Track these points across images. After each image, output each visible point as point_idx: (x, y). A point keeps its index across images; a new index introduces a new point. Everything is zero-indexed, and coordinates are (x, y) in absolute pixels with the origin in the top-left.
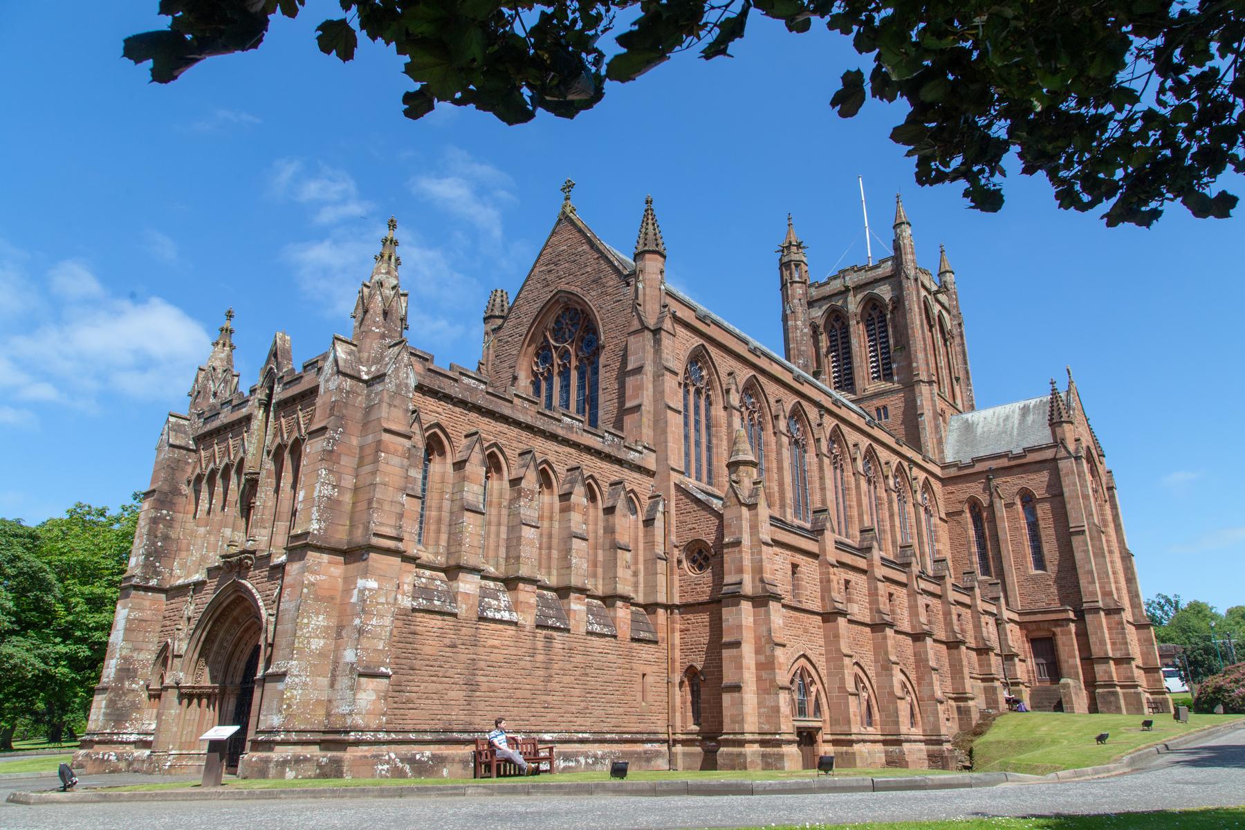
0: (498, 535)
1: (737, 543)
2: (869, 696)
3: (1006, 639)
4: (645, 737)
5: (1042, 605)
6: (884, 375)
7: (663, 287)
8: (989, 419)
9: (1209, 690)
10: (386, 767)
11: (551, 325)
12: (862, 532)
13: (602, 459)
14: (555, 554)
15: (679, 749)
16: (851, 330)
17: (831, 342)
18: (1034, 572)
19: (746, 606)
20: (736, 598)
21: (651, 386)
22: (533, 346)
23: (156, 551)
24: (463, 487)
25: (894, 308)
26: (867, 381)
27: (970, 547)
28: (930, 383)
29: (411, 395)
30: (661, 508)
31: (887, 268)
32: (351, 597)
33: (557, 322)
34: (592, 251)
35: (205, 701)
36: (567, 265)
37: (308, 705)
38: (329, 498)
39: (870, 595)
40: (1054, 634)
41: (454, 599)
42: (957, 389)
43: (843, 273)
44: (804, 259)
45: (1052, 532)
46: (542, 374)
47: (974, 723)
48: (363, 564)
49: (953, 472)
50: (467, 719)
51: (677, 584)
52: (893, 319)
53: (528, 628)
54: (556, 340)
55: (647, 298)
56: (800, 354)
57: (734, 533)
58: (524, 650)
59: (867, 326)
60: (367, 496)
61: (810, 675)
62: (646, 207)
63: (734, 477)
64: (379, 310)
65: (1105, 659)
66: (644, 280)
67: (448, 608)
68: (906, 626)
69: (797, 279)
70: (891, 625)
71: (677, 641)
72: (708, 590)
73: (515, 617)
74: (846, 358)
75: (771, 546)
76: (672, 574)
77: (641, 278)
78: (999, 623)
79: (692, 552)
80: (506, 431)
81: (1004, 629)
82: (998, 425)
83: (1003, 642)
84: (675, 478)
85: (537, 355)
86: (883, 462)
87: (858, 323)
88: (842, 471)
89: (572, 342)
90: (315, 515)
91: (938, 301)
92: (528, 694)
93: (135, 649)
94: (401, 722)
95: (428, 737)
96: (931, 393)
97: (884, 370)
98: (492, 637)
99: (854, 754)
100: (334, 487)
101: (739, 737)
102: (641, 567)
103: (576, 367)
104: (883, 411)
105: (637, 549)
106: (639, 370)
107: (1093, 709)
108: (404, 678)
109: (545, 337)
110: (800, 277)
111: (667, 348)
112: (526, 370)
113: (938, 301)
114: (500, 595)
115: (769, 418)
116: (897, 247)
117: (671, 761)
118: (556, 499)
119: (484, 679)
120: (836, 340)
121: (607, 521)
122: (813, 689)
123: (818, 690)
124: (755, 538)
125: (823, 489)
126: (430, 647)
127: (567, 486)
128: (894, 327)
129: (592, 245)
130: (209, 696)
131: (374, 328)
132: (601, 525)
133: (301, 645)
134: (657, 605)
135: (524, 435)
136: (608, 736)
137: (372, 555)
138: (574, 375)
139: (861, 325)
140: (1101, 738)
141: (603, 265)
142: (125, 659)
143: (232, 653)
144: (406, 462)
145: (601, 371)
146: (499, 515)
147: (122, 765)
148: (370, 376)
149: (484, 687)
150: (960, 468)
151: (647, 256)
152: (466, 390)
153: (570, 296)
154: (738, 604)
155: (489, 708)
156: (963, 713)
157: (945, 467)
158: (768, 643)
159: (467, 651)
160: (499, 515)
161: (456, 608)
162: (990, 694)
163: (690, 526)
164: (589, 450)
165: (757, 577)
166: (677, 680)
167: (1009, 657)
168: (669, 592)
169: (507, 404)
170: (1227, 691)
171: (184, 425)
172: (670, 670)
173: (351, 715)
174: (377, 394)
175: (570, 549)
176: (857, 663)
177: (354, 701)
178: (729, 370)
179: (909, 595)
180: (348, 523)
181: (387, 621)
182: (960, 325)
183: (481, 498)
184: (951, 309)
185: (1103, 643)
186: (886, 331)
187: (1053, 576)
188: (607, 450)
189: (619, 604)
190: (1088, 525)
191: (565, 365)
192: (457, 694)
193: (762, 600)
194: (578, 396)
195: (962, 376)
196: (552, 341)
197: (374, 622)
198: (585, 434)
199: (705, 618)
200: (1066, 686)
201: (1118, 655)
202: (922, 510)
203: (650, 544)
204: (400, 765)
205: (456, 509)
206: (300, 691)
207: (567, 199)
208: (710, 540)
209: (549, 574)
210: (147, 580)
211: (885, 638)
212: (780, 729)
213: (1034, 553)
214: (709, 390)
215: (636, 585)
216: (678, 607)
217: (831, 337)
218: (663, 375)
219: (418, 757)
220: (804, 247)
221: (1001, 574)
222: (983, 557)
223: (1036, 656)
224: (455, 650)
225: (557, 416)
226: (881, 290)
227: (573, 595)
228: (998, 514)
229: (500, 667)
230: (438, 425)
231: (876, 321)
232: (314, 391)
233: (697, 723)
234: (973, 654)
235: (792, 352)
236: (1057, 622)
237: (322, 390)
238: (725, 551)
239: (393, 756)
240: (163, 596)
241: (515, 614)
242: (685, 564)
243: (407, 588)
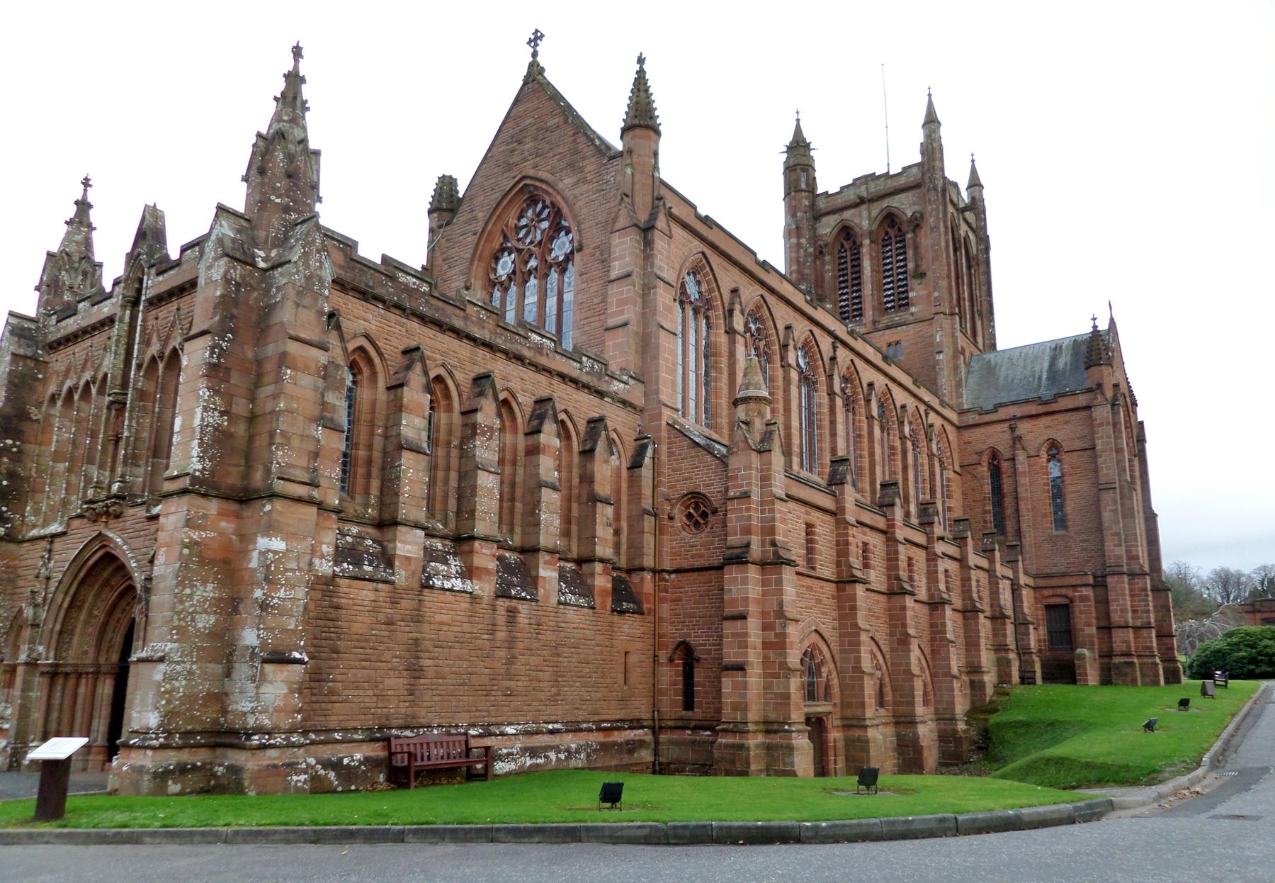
0: (446, 481)
1: (746, 496)
2: (882, 674)
3: (1022, 607)
10: (303, 777)
14: (519, 506)
19: (753, 573)
24: (400, 419)
29: (327, 293)
30: (649, 453)
32: (250, 561)
37: (196, 699)
38: (216, 429)
41: (390, 563)
42: (979, 323)
47: (988, 698)
50: (409, 711)
53: (486, 600)
55: (636, 187)
58: (481, 626)
60: (267, 428)
61: (821, 652)
67: (382, 574)
70: (912, 594)
73: (468, 586)
75: (786, 501)
81: (1020, 596)
83: (1018, 609)
88: (854, 414)
90: (195, 451)
92: (485, 679)
94: (323, 718)
100: (222, 414)
102: (624, 524)
105: (619, 500)
107: (1106, 680)
108: (323, 664)
111: (661, 253)
114: (450, 558)
115: (776, 347)
118: (521, 436)
119: (429, 662)
120: (846, 262)
122: (824, 670)
123: (829, 671)
125: (833, 435)
126: (359, 624)
131: (273, 197)
132: (576, 472)
133: (182, 623)
135: (481, 353)
144: (320, 383)
146: (448, 457)
148: (269, 264)
149: (430, 672)
152: (404, 291)
155: (437, 698)
157: (962, 412)
158: (776, 618)
159: (407, 629)
160: (448, 457)
161: (393, 574)
164: (563, 377)
168: (657, 554)
169: (458, 312)
171: (30, 329)
173: (253, 713)
174: (279, 289)
175: (539, 502)
177: (257, 697)
178: (733, 286)
180: (243, 462)
181: (300, 592)
183: (424, 435)
188: (585, 378)
190: (1120, 481)
192: (395, 683)
197: (282, 594)
198: (558, 357)
200: (1082, 657)
201: (1138, 623)
203: (635, 494)
204: (322, 772)
205: (390, 448)
206: (184, 683)
209: (512, 531)
212: (790, 719)
214: (708, 309)
215: (617, 546)
218: (655, 287)
219: (346, 761)
224: (392, 628)
229: (450, 647)
230: (367, 337)
231: (893, 240)
232: (193, 284)
237: (201, 282)
239: (312, 761)
241: (468, 582)
243: (327, 549)
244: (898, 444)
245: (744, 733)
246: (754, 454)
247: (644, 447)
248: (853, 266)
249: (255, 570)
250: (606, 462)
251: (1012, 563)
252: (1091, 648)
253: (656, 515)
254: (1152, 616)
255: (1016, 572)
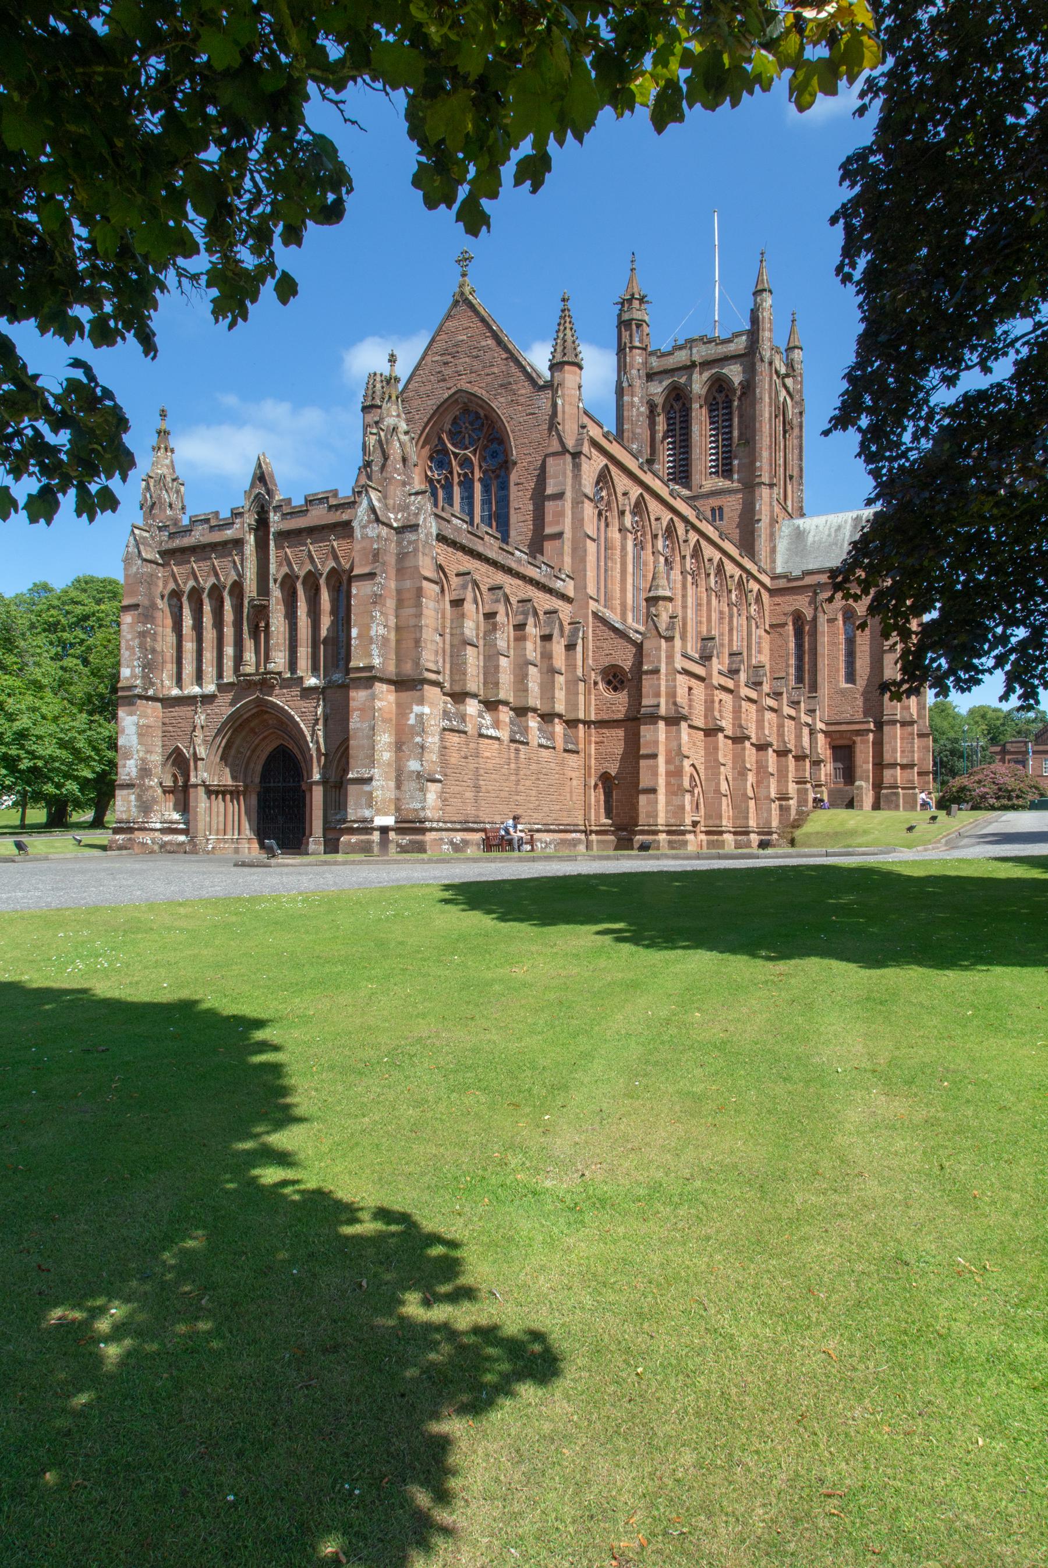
1: (656, 671)
3: (816, 747)
4: (572, 828)
5: (846, 716)
6: (723, 471)
7: (581, 405)
8: (821, 528)
9: (954, 789)
11: (447, 427)
12: (731, 655)
13: (539, 589)
15: (593, 837)
16: (693, 414)
17: (668, 425)
18: (844, 685)
19: (661, 724)
20: (653, 718)
21: (570, 512)
22: (428, 447)
23: (149, 664)
25: (743, 394)
26: (705, 479)
27: (788, 659)
28: (771, 486)
31: (740, 344)
32: (408, 719)
33: (455, 422)
34: (498, 349)
35: (228, 797)
36: (467, 359)
39: (734, 712)
40: (854, 742)
41: (464, 720)
42: (789, 487)
43: (690, 343)
44: (646, 318)
45: (867, 648)
46: (439, 481)
48: (418, 693)
49: (782, 583)
51: (593, 702)
52: (739, 407)
54: (453, 445)
55: (566, 416)
56: (634, 438)
57: (653, 662)
59: (711, 411)
62: (561, 305)
63: (653, 610)
64: (399, 457)
65: (894, 765)
66: (563, 396)
67: (462, 727)
68: (700, 722)
69: (637, 344)
71: (593, 752)
72: (623, 710)
74: (684, 447)
76: (590, 694)
77: (560, 392)
78: (812, 732)
79: (608, 675)
80: (479, 567)
81: (816, 738)
82: (829, 535)
84: (593, 606)
85: (431, 458)
86: (728, 575)
87: (701, 407)
89: (475, 450)
91: (785, 386)
93: (147, 752)
95: (458, 826)
96: (771, 498)
97: (723, 465)
98: (488, 749)
99: (723, 841)
101: (653, 828)
103: (480, 479)
104: (717, 513)
106: (560, 496)
107: (876, 806)
109: (440, 439)
110: (641, 341)
112: (420, 475)
113: (785, 386)
115: (649, 537)
116: (755, 319)
117: (588, 847)
121: (543, 647)
124: (670, 667)
127: (521, 617)
128: (740, 417)
129: (499, 342)
130: (231, 793)
134: (578, 721)
136: (552, 827)
137: (426, 687)
138: (478, 487)
139: (704, 410)
140: (910, 829)
141: (514, 369)
142: (143, 760)
143: (250, 758)
145: (513, 489)
147: (156, 848)
149: (483, 790)
150: (789, 580)
151: (567, 368)
153: (473, 398)
154: (656, 723)
156: (784, 810)
158: (677, 755)
162: (802, 794)
163: (607, 652)
165: (671, 701)
166: (593, 783)
167: (817, 763)
170: (970, 791)
172: (587, 775)
175: (527, 675)
176: (693, 765)
179: (757, 711)
182: (801, 413)
183: (474, 632)
184: (794, 394)
185: (894, 751)
186: (731, 420)
187: (861, 689)
188: (543, 580)
189: (557, 720)
191: (466, 475)
192: (469, 795)
193: (674, 721)
194: (483, 510)
195: (795, 474)
196: (449, 446)
199: (620, 733)
200: (860, 788)
201: (905, 762)
202: (753, 623)
205: (456, 642)
207: (464, 275)
208: (627, 665)
210: (146, 690)
211: (744, 749)
213: (847, 668)
216: (594, 723)
217: (668, 419)
218: (583, 503)
220: (647, 302)
221: (814, 687)
222: (800, 669)
223: (835, 760)
225: (510, 549)
226: (731, 371)
227: (530, 714)
228: (820, 628)
231: (721, 406)
233: (608, 815)
234: (754, 750)
235: (626, 434)
236: (858, 733)
238: (644, 677)
240: (159, 704)
242: (601, 686)
244: (726, 609)
245: (656, 833)
246: (663, 640)
247: (577, 630)
248: (681, 428)
249: (413, 726)
250: (558, 643)
251: (811, 712)
252: (867, 781)
253: (585, 681)
254: (916, 755)
255: (814, 719)
